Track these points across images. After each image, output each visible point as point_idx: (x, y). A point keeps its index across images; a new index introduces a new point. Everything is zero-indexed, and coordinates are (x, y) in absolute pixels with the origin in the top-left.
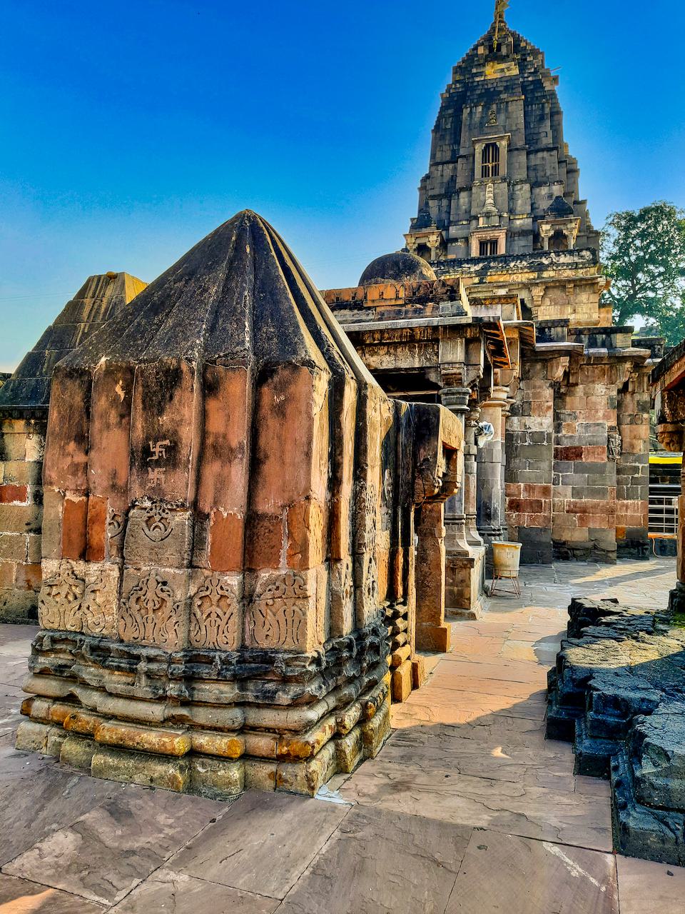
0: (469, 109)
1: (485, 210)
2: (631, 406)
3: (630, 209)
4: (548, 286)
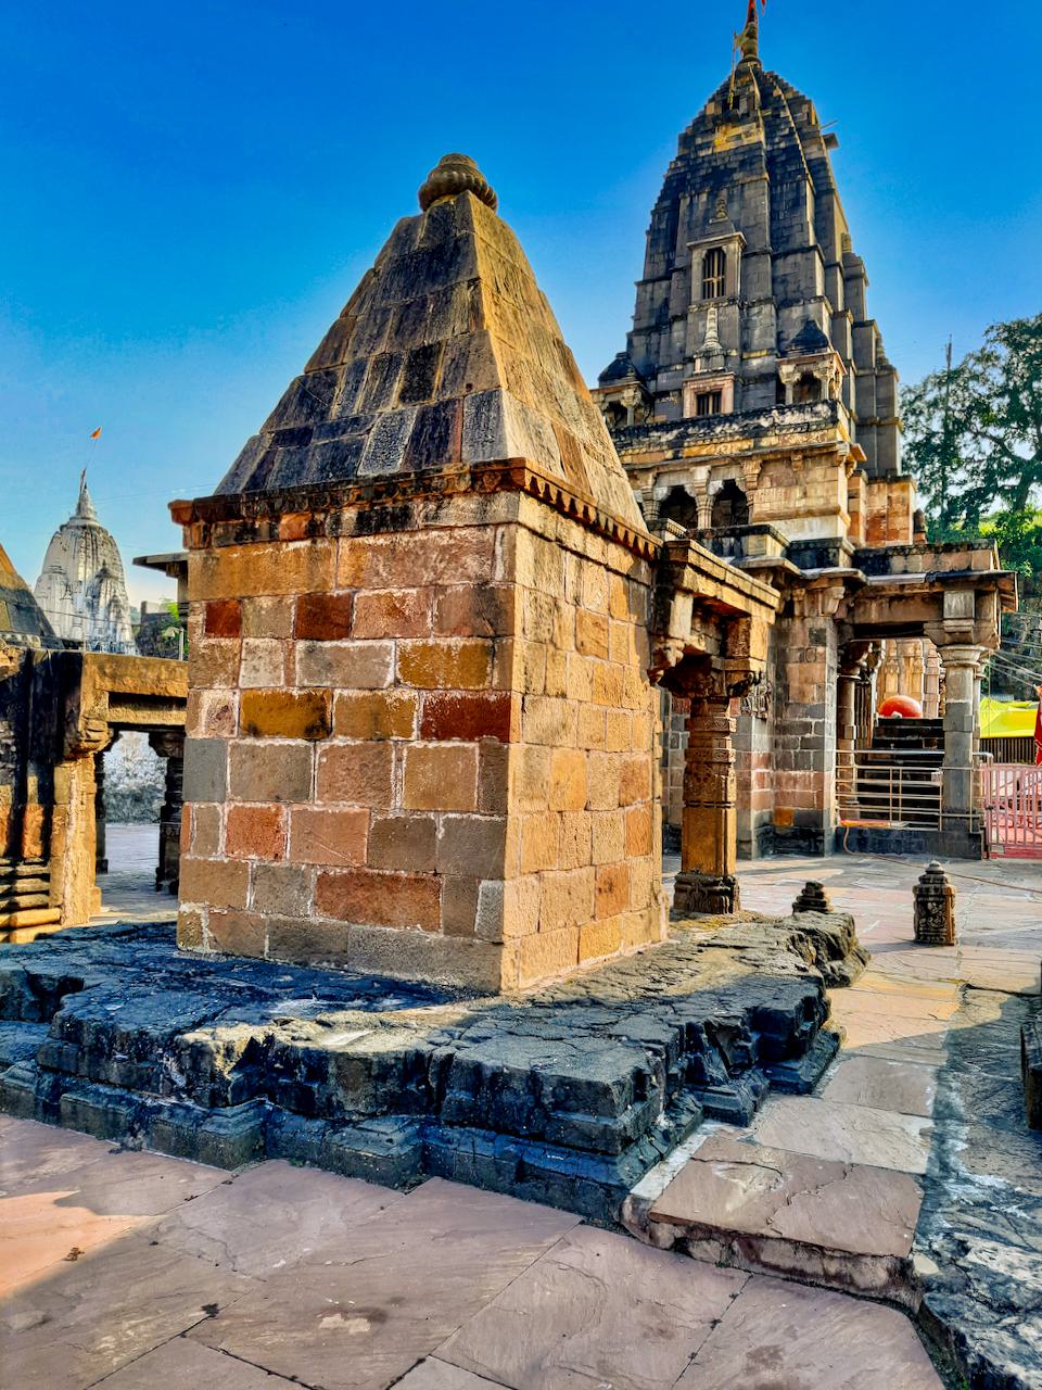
0: (688, 200)
1: (703, 348)
2: (801, 635)
3: (1022, 317)
4: (767, 461)
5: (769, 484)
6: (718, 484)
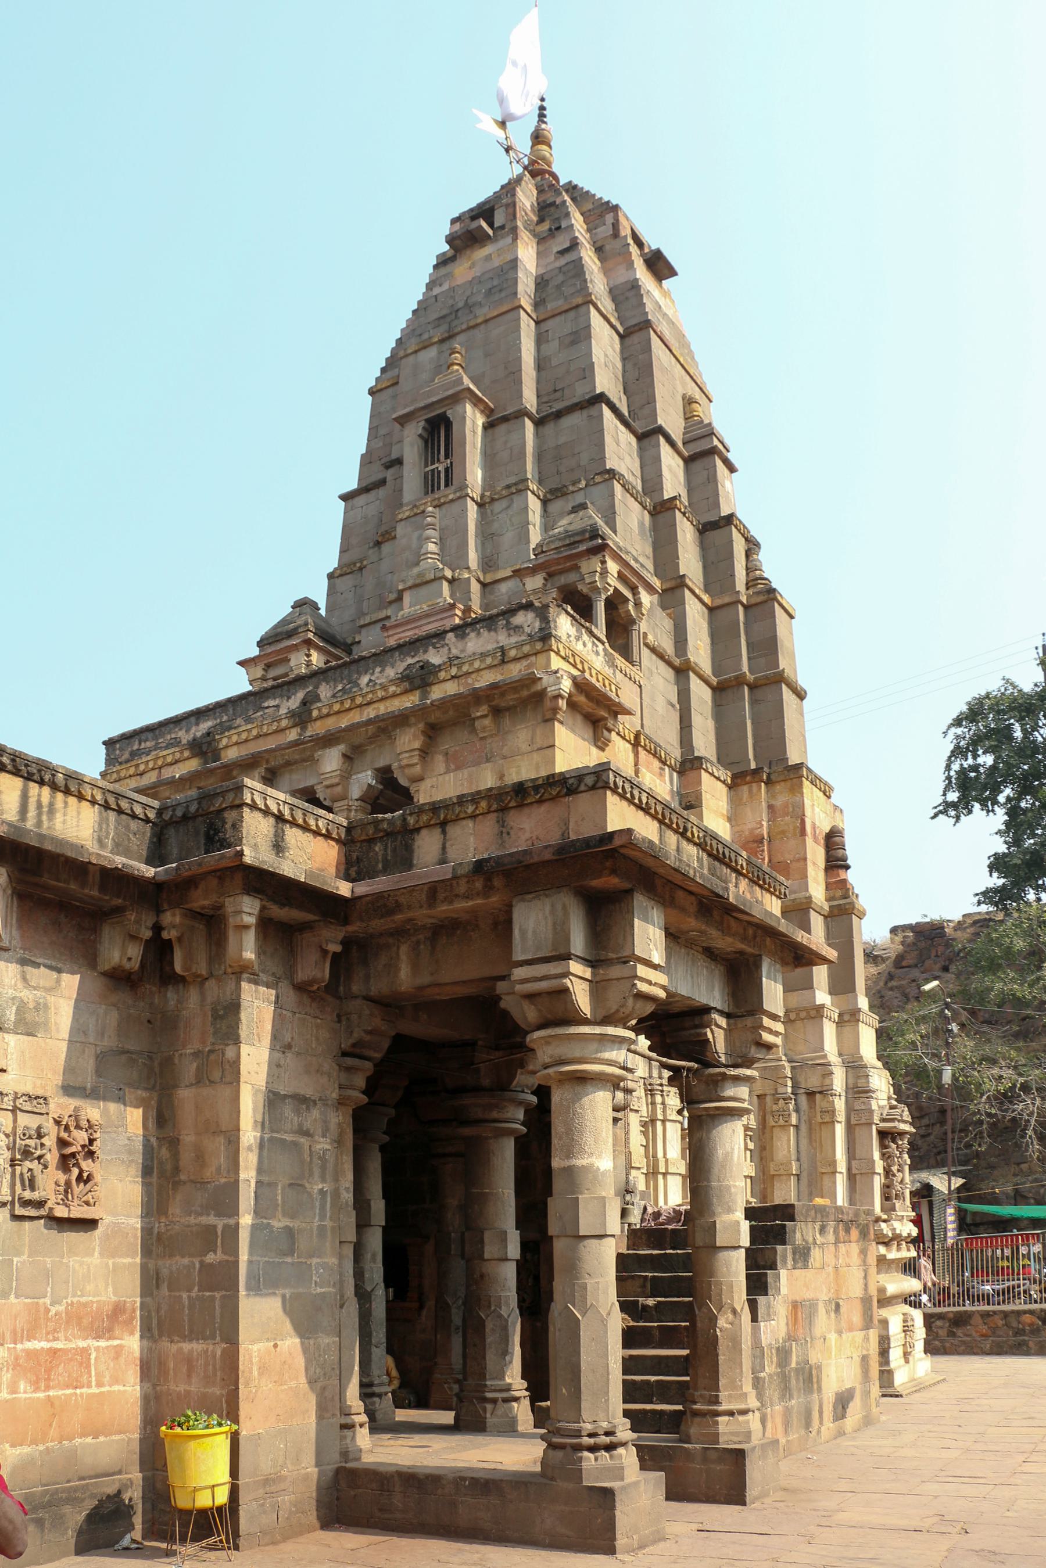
6: (365, 779)
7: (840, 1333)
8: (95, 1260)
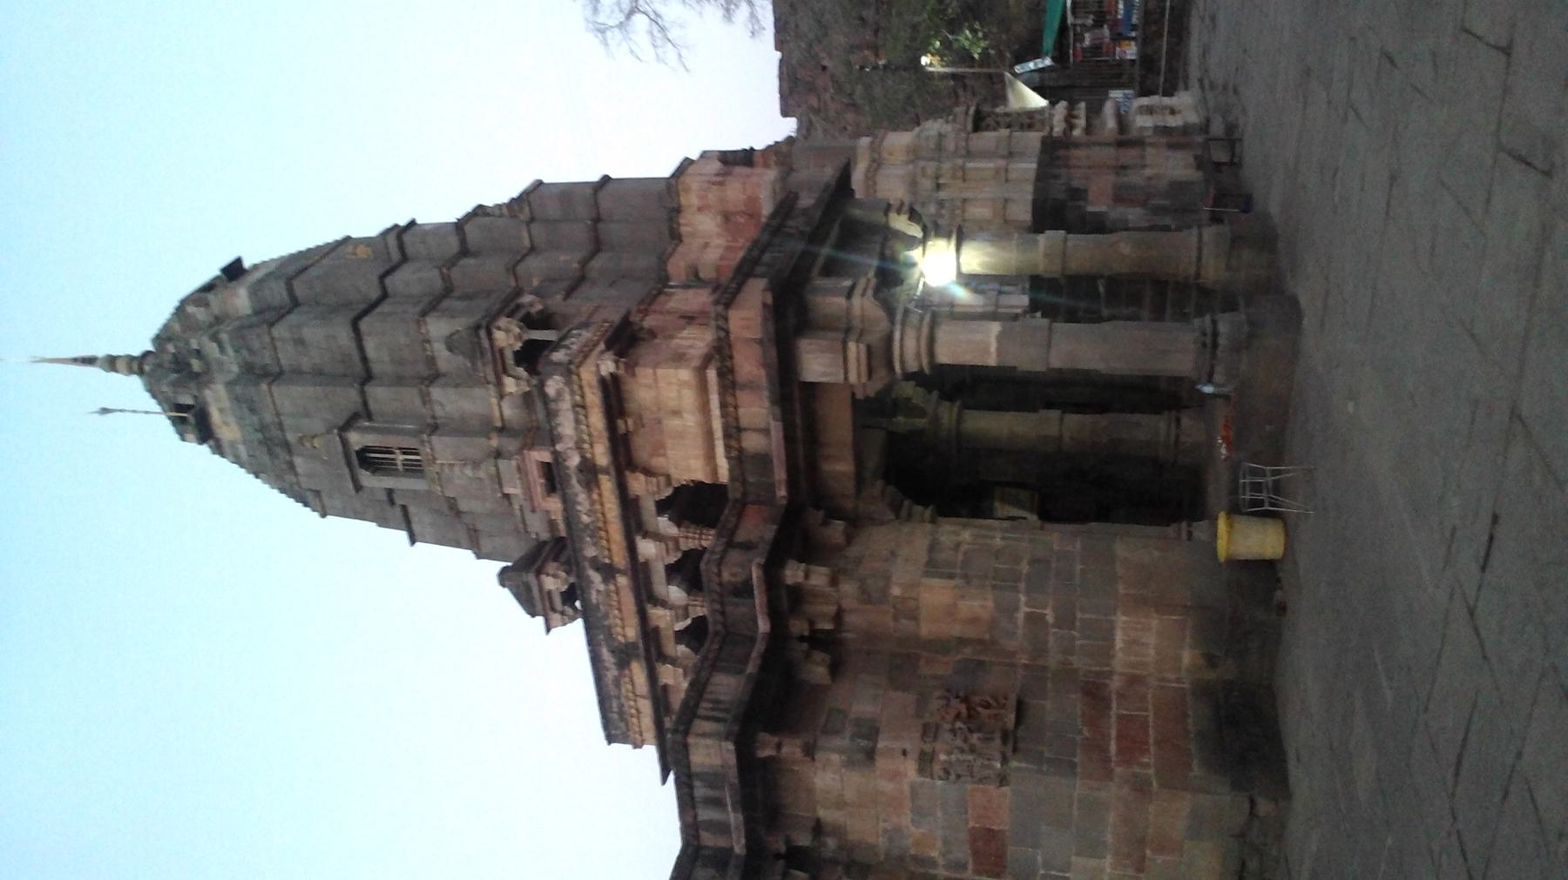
5: (661, 459)
6: (664, 524)
7: (1144, 166)
8: (1048, 705)
